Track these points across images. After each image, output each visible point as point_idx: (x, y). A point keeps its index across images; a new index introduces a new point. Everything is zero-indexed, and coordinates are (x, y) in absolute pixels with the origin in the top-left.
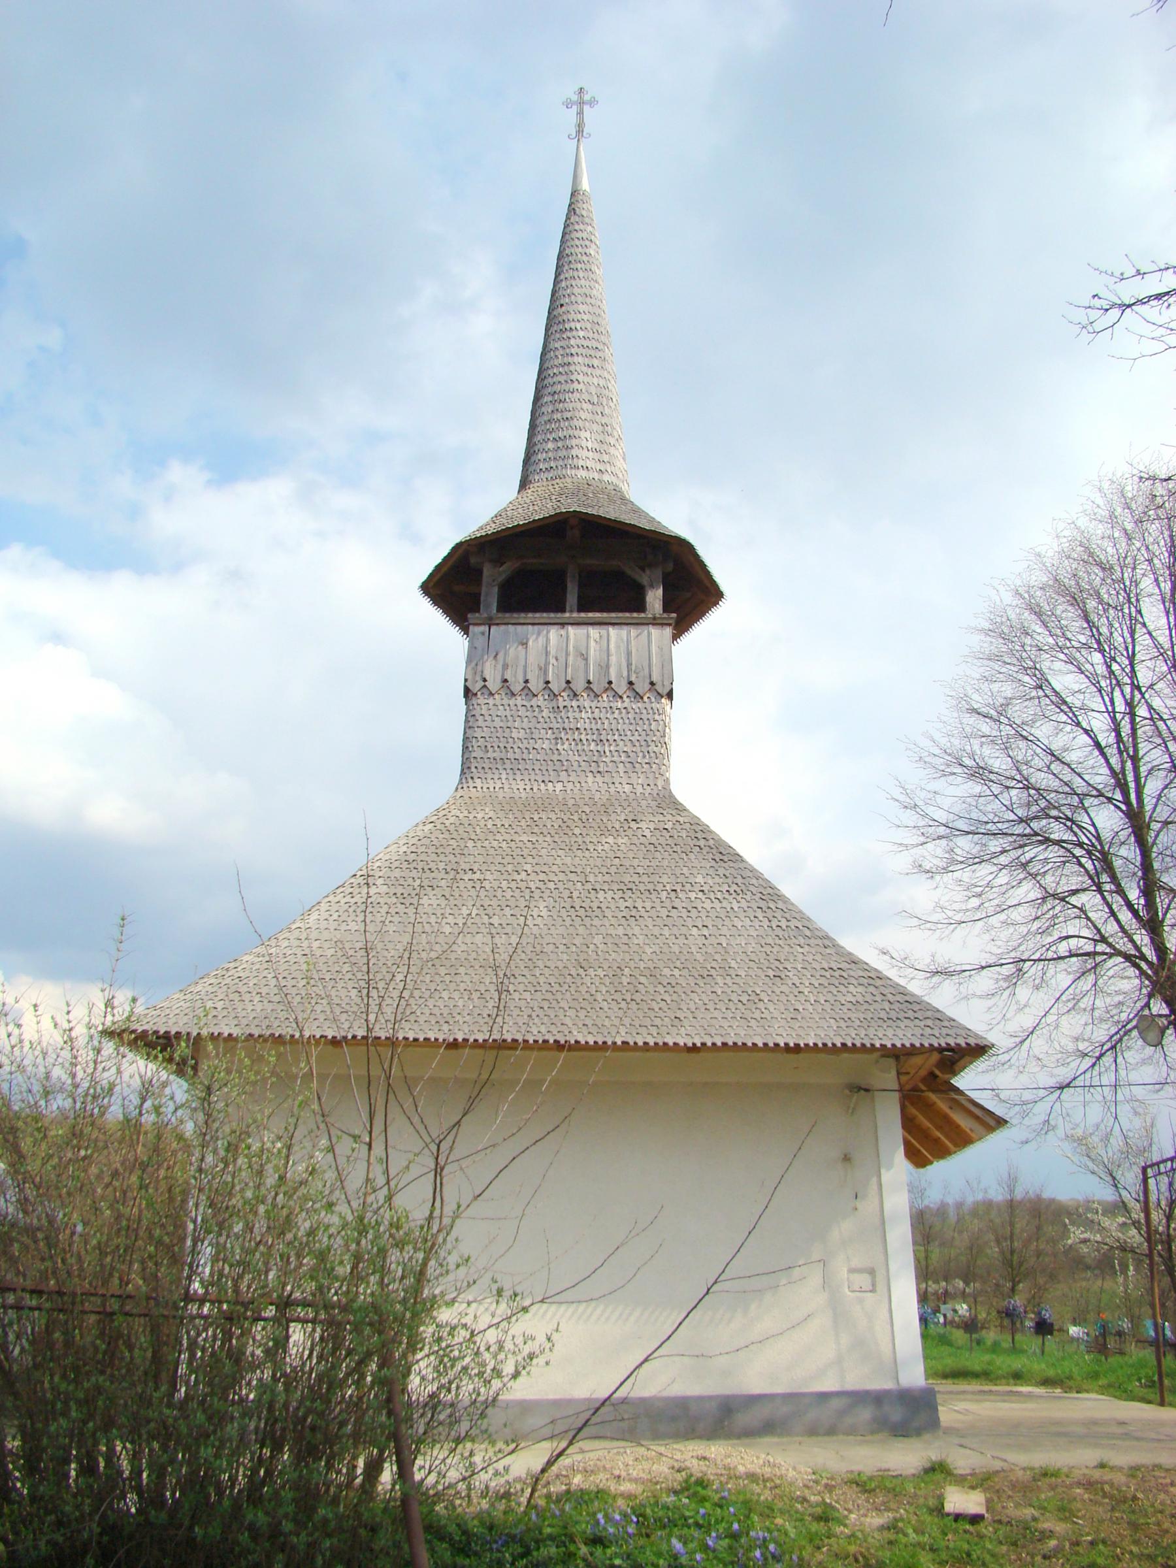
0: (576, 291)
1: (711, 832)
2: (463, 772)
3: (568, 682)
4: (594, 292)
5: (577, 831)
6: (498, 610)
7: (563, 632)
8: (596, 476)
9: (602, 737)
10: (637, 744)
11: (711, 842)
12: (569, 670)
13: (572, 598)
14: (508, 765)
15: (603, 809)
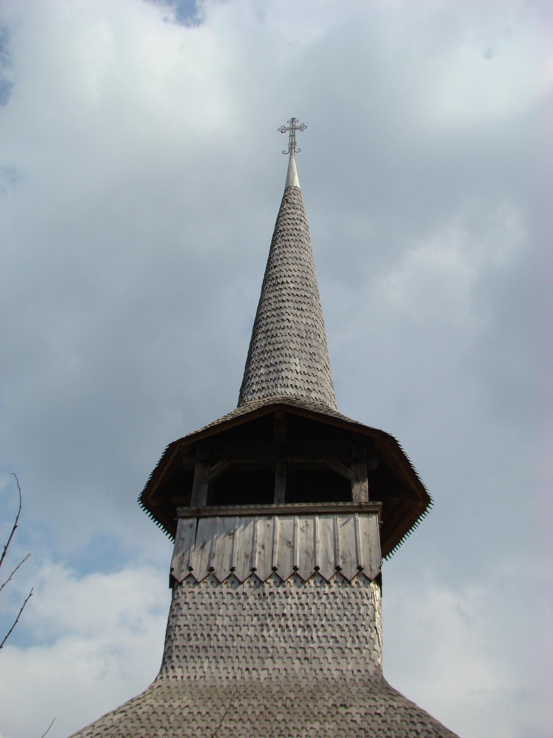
0: (287, 255)
1: (428, 716)
2: (164, 663)
3: (274, 569)
4: (304, 256)
5: (280, 717)
6: (209, 503)
7: (270, 522)
8: (305, 393)
9: (309, 623)
10: (346, 629)
11: (429, 727)
12: (276, 558)
13: (280, 491)
14: (211, 653)
15: (310, 695)
